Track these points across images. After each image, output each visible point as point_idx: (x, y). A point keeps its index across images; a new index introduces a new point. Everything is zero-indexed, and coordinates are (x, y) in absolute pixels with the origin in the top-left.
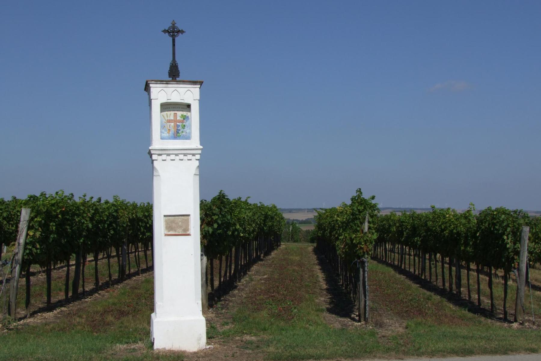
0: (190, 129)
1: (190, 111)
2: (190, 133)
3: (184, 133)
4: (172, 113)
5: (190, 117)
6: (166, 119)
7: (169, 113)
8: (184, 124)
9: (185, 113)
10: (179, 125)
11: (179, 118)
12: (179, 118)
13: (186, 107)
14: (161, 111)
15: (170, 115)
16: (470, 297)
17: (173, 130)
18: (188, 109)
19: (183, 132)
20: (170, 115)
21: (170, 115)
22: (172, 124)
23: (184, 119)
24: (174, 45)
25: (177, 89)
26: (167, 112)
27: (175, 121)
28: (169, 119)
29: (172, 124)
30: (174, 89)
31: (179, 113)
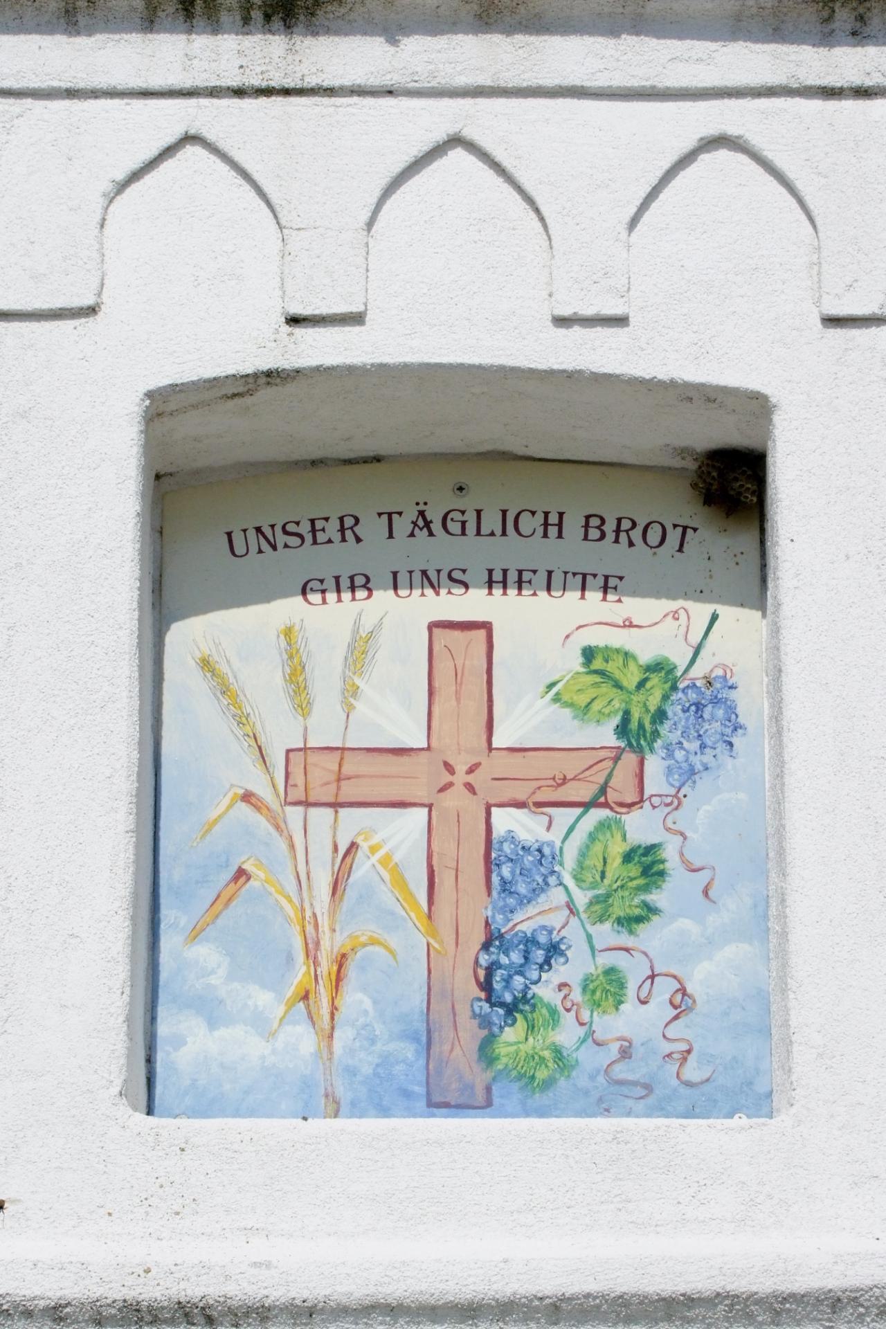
0: (766, 924)
1: (756, 587)
2: (761, 1015)
3: (635, 1020)
4: (401, 617)
5: (750, 701)
6: (282, 732)
7: (329, 620)
8: (641, 827)
9: (653, 626)
10: (543, 858)
11: (523, 719)
12: (523, 719)
13: (679, 506)
14: (164, 598)
15: (360, 651)
16: (592, 1012)
17: (402, 961)
18: (715, 542)
19: (608, 988)
20: (349, 654)
21: (360, 651)
22: (403, 833)
23: (635, 736)
24: (330, 92)
25: (487, 121)
26: (290, 608)
27: (454, 770)
28: (325, 730)
29: (403, 833)
30: (432, 120)
31: (542, 631)
